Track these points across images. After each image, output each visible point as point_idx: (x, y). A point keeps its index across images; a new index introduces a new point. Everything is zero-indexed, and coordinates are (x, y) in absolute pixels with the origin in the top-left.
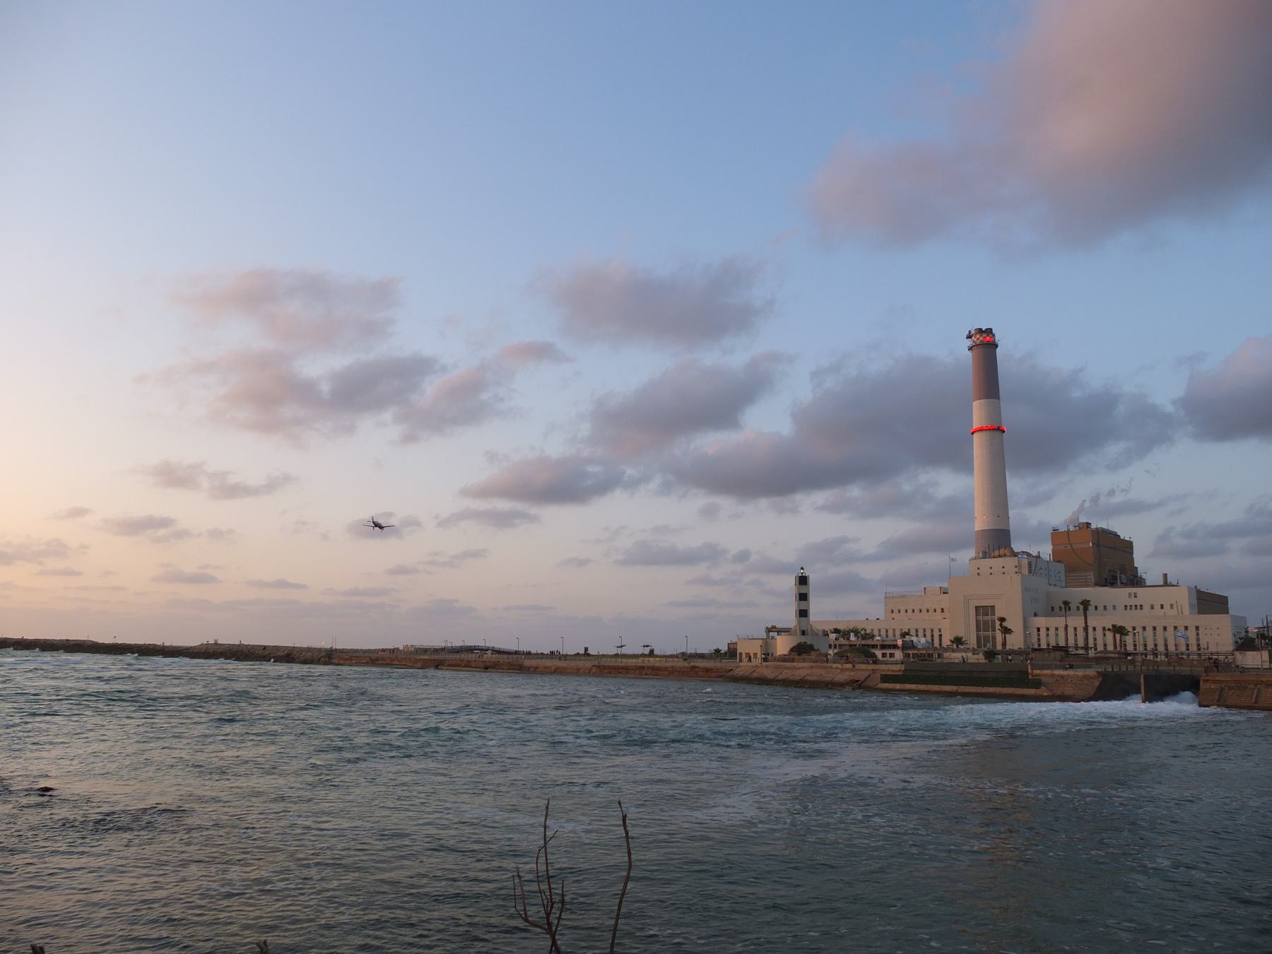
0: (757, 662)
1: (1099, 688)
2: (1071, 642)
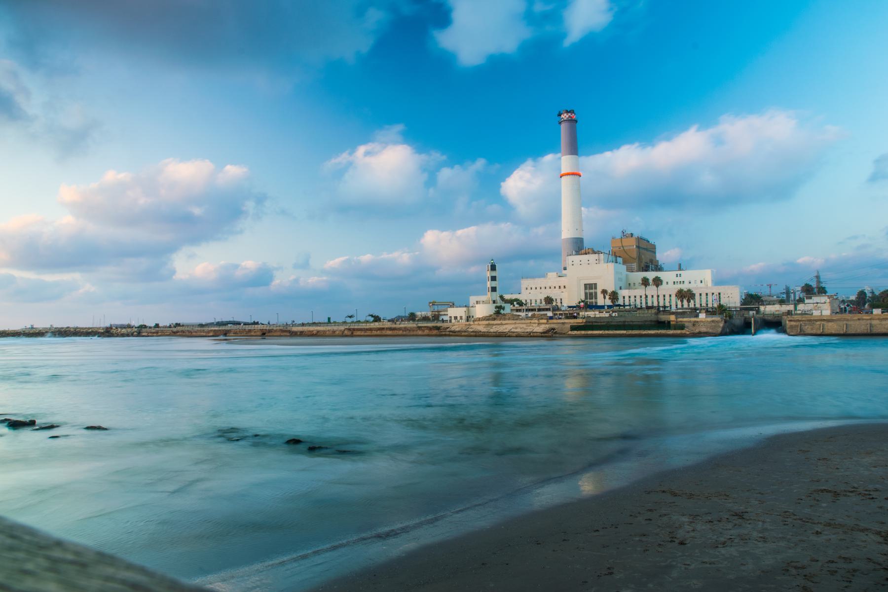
0: (464, 321)
1: (723, 328)
2: (661, 304)
